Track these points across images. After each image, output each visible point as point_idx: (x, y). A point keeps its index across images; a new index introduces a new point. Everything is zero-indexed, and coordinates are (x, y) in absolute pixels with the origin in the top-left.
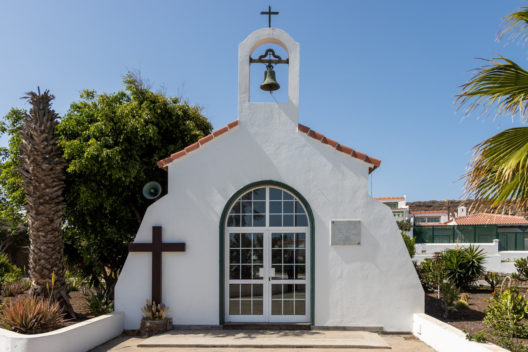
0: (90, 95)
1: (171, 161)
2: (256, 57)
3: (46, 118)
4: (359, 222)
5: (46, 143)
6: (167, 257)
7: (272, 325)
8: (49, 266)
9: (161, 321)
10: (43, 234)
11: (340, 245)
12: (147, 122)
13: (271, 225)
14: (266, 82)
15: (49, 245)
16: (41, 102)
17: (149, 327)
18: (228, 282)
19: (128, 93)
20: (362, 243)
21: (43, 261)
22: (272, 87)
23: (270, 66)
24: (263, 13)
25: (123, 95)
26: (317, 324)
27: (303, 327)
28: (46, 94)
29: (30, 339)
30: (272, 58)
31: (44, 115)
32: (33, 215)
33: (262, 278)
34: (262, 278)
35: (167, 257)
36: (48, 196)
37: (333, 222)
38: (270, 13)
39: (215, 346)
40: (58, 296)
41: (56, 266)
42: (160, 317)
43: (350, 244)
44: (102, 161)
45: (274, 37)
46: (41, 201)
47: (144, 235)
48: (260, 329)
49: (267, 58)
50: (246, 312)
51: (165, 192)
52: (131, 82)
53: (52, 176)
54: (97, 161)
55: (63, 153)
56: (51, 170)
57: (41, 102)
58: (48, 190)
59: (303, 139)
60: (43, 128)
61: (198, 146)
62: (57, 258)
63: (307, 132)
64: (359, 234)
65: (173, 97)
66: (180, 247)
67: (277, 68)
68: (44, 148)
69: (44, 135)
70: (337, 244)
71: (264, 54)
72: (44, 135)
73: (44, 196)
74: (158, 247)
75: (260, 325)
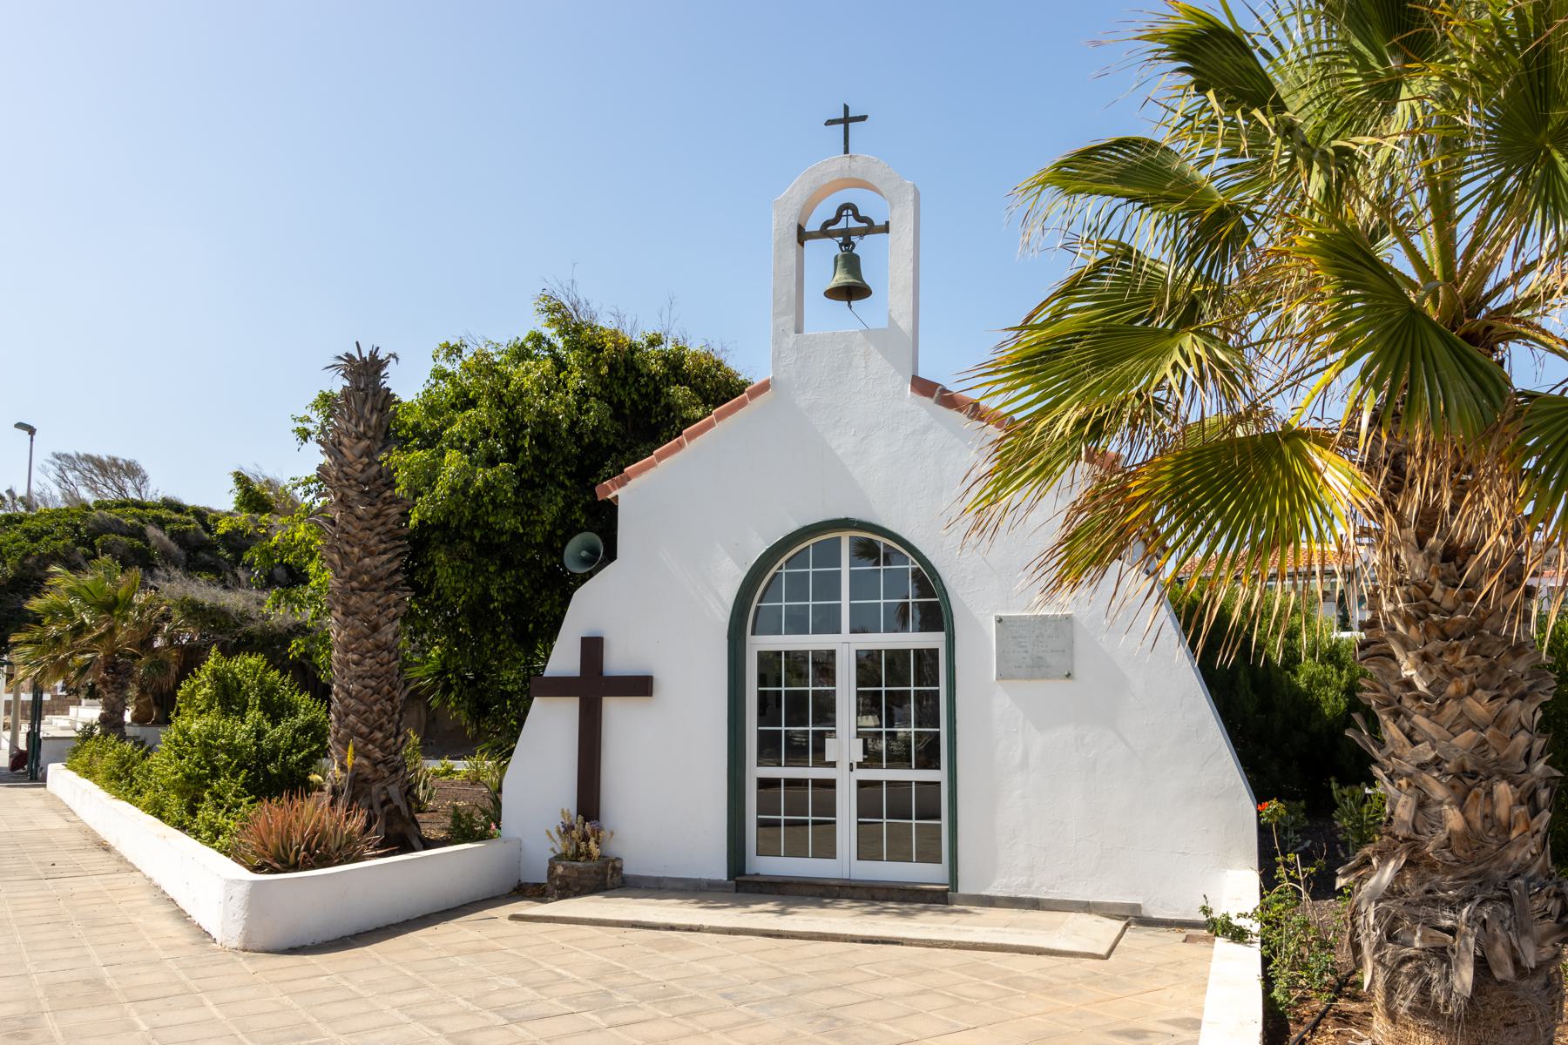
0: (453, 351)
1: (622, 484)
2: (813, 225)
3: (368, 406)
4: (1068, 618)
5: (365, 460)
6: (615, 709)
7: (854, 888)
8: (364, 729)
9: (589, 864)
10: (355, 657)
11: (1020, 678)
12: (583, 394)
13: (853, 631)
14: (833, 284)
15: (368, 681)
16: (366, 372)
17: (562, 877)
18: (755, 772)
19: (549, 333)
20: (1077, 673)
21: (352, 718)
22: (853, 292)
23: (847, 244)
24: (830, 123)
25: (538, 339)
26: (964, 888)
27: (929, 896)
28: (373, 355)
29: (255, 883)
30: (853, 224)
31: (365, 402)
32: (339, 615)
33: (833, 764)
34: (833, 764)
35: (615, 709)
36: (367, 572)
37: (1000, 620)
38: (847, 120)
39: (672, 928)
40: (383, 797)
41: (380, 728)
42: (589, 855)
43: (1045, 677)
44: (478, 495)
45: (854, 176)
46: (354, 584)
47: (564, 659)
48: (823, 896)
49: (841, 225)
50: (796, 851)
51: (611, 555)
52: (556, 311)
53: (379, 529)
54: (465, 493)
55: (392, 484)
56: (377, 516)
57: (366, 372)
58: (367, 560)
59: (924, 413)
60: (361, 429)
61: (680, 445)
62: (384, 711)
63: (931, 396)
64: (1068, 650)
65: (650, 333)
66: (640, 686)
67: (864, 247)
68: (363, 471)
69: (364, 443)
70: (1012, 677)
71: (832, 215)
72: (364, 443)
73: (360, 574)
74: (596, 685)
75: (824, 885)
